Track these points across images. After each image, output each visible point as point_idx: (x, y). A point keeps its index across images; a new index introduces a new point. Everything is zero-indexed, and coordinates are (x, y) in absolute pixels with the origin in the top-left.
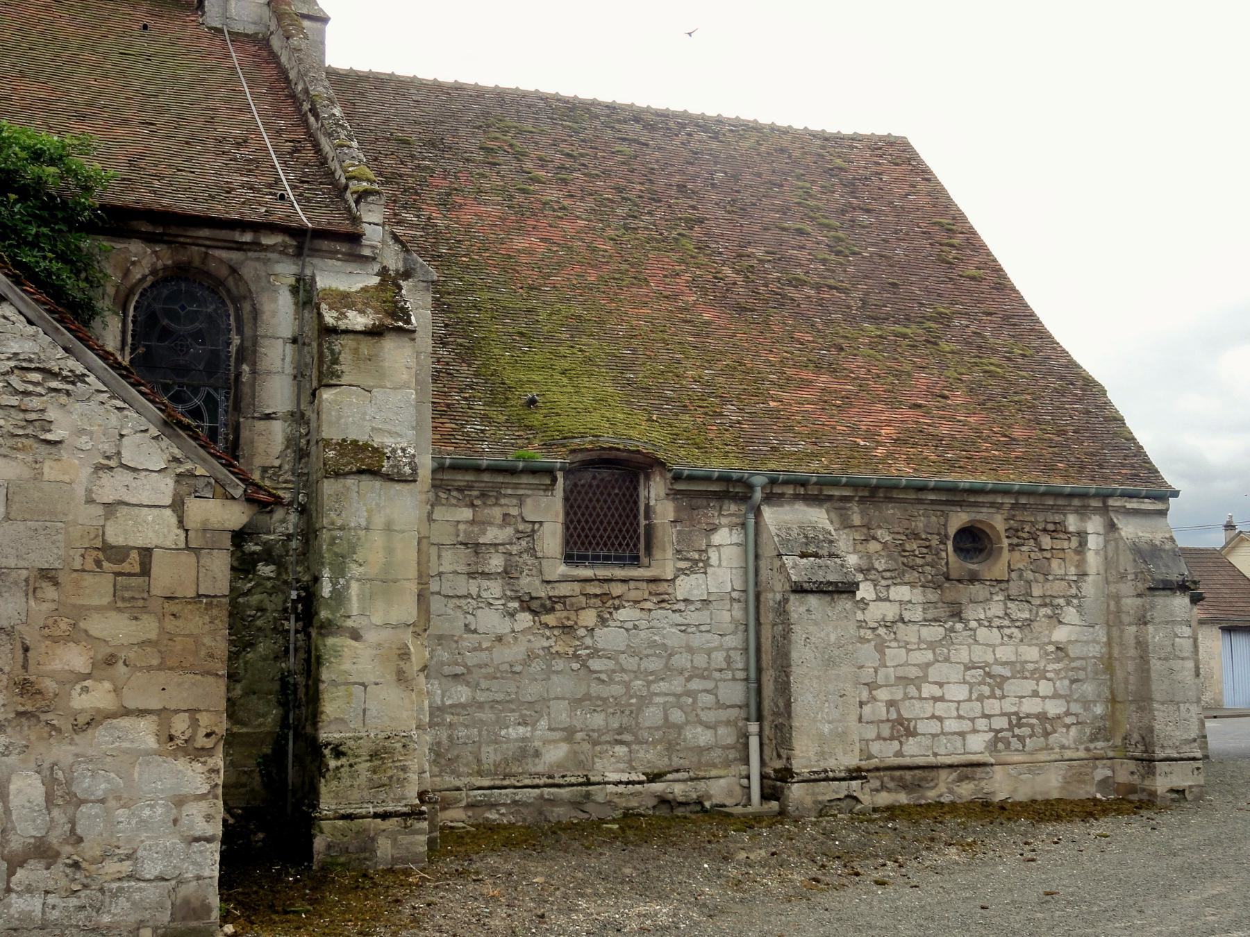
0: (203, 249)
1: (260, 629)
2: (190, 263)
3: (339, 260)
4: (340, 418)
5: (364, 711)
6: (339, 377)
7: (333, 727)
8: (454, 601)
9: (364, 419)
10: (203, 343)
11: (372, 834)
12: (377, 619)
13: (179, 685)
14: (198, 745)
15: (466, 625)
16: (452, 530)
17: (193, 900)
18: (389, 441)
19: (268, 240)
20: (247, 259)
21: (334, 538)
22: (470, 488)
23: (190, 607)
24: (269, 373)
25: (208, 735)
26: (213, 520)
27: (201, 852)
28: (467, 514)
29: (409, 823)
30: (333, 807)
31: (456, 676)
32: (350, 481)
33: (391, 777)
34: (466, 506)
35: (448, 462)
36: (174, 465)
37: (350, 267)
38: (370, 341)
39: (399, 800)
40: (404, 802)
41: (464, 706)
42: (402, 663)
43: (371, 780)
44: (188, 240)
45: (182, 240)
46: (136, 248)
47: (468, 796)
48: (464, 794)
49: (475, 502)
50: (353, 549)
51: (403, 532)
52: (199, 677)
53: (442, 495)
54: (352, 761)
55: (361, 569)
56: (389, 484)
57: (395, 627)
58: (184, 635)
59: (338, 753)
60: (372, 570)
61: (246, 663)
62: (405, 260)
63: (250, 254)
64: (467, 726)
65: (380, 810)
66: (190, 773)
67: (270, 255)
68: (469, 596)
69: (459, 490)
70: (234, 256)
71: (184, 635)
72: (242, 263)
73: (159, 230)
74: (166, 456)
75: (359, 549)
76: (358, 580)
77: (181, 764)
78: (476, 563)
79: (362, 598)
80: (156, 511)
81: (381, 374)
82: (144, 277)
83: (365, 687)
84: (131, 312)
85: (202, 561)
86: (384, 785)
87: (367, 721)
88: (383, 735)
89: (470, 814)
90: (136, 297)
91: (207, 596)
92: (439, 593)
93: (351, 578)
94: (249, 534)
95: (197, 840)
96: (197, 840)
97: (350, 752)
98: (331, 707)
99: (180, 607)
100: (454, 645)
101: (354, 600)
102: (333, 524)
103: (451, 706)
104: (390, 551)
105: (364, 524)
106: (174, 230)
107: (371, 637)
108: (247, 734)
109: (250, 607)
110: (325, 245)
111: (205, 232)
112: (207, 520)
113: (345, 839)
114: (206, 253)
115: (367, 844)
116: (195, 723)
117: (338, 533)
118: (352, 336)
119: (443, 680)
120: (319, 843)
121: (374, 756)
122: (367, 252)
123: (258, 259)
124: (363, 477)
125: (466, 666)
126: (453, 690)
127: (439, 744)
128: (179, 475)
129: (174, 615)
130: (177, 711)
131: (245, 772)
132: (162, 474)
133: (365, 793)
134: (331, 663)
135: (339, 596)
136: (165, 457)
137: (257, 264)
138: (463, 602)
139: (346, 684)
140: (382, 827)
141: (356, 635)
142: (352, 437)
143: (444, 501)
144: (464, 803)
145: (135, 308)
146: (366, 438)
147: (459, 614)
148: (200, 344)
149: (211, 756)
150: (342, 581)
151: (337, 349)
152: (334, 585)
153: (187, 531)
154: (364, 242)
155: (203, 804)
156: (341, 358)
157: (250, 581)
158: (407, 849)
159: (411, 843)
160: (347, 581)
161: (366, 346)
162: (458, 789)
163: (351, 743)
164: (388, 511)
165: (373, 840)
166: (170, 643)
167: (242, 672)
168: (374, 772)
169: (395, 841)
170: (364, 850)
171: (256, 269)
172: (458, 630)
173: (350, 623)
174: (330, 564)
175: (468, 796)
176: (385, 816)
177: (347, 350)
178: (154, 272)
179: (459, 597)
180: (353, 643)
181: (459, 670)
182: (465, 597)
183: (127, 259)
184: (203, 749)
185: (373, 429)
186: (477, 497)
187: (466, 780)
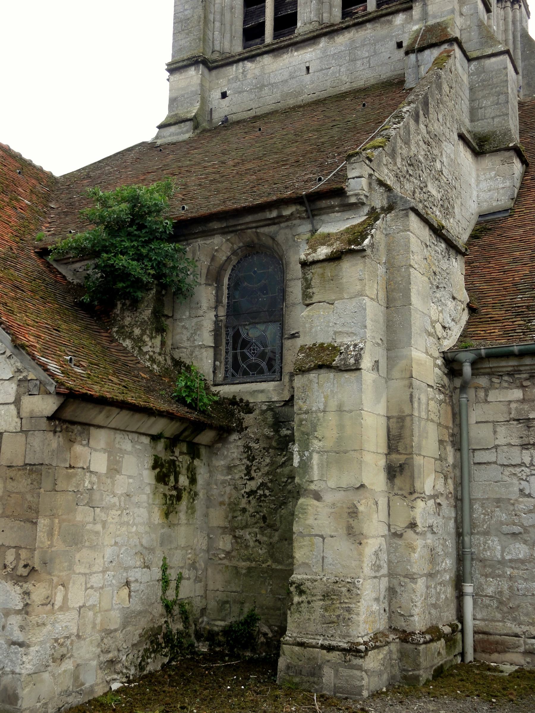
0: (254, 230)
1: (290, 492)
2: (253, 242)
3: (338, 212)
4: (311, 328)
5: (323, 558)
6: (311, 297)
7: (301, 570)
8: (510, 469)
9: (328, 326)
10: (267, 293)
11: (320, 662)
12: (332, 484)
13: (12, 528)
14: (19, 573)
15: (521, 490)
16: (505, 409)
17: (9, 689)
18: (347, 340)
19: (287, 212)
20: (280, 229)
21: (301, 420)
22: (519, 372)
23: (20, 472)
24: (294, 305)
25: (25, 566)
26: (36, 410)
27: (16, 653)
28: (518, 394)
29: (348, 658)
30: (294, 635)
31: (514, 534)
32: (313, 375)
33: (338, 616)
34: (517, 387)
35: (483, 352)
36: (18, 374)
37: (346, 215)
38: (332, 265)
39: (344, 637)
40: (348, 639)
41: (522, 562)
42: (351, 520)
43: (323, 616)
44: (243, 227)
45: (239, 228)
46: (217, 240)
47: (525, 643)
48: (522, 641)
49: (525, 383)
50: (314, 428)
51: (351, 411)
52: (22, 523)
53: (494, 380)
54: (309, 599)
55: (320, 444)
56: (340, 374)
57: (346, 490)
58: (17, 493)
59: (301, 593)
60: (328, 444)
61: (281, 517)
62: (388, 197)
63: (282, 225)
64: (526, 580)
65: (326, 643)
66: (13, 593)
67: (295, 222)
68: (522, 464)
69: (509, 374)
70: (273, 229)
71: (17, 493)
72: (277, 232)
73: (224, 225)
74: (14, 369)
75: (319, 428)
76: (318, 452)
77: (8, 586)
78: (528, 436)
79: (321, 466)
80: (6, 407)
81: (340, 289)
82: (228, 258)
83: (324, 539)
84: (226, 281)
85: (28, 440)
86: (334, 622)
87: (325, 567)
88: (333, 579)
89: (528, 660)
90: (229, 272)
91: (30, 465)
92: (495, 463)
93: (313, 451)
94: (283, 422)
95: (14, 643)
96: (14, 643)
97: (308, 591)
98: (300, 554)
99: (15, 472)
100: (512, 508)
101: (315, 467)
102: (300, 409)
103: (511, 561)
104: (341, 427)
105: (322, 407)
106: (232, 222)
107: (328, 498)
108: (281, 570)
109: (284, 475)
110: (324, 203)
111: (249, 218)
112: (33, 410)
113: (300, 663)
114: (256, 232)
115: (315, 672)
116: (18, 557)
117: (304, 416)
118: (319, 265)
119: (503, 538)
120: (282, 663)
121: (326, 596)
122: (353, 200)
123: (287, 227)
124: (322, 371)
125: (522, 526)
126: (512, 546)
127: (501, 593)
128: (20, 381)
129: (11, 478)
130: (9, 547)
131: (279, 599)
132: (11, 381)
133: (319, 627)
134: (299, 518)
135: (305, 465)
136: (13, 369)
137: (287, 231)
138: (518, 470)
139: (310, 535)
140: (327, 658)
141: (317, 497)
142: (319, 341)
143: (497, 386)
144: (522, 649)
145: (229, 279)
146: (330, 340)
147: (515, 481)
148: (264, 294)
149: (26, 582)
150: (307, 454)
151: (309, 277)
152: (301, 457)
153: (22, 419)
154: (349, 193)
155: (19, 617)
156: (312, 284)
157: (285, 456)
158: (347, 681)
159: (350, 676)
160: (311, 454)
161: (329, 270)
162: (517, 636)
163: (308, 584)
164: (340, 396)
165: (320, 667)
166: (9, 498)
167: (278, 524)
168: (326, 610)
169: (337, 671)
170: (313, 675)
171: (286, 234)
172: (514, 495)
173: (313, 487)
174: (299, 440)
175: (525, 643)
176: (330, 649)
177: (316, 276)
178: (234, 253)
179: (514, 466)
180: (315, 502)
181: (517, 529)
182: (519, 465)
183: (213, 249)
184: (21, 576)
185: (335, 333)
186: (526, 379)
187: (524, 628)
